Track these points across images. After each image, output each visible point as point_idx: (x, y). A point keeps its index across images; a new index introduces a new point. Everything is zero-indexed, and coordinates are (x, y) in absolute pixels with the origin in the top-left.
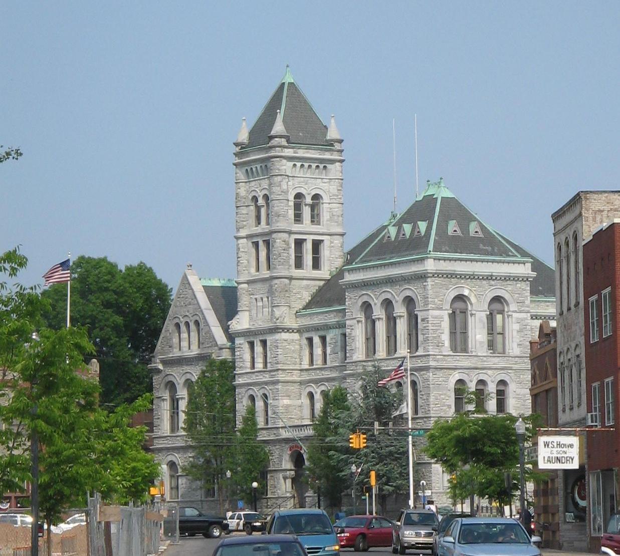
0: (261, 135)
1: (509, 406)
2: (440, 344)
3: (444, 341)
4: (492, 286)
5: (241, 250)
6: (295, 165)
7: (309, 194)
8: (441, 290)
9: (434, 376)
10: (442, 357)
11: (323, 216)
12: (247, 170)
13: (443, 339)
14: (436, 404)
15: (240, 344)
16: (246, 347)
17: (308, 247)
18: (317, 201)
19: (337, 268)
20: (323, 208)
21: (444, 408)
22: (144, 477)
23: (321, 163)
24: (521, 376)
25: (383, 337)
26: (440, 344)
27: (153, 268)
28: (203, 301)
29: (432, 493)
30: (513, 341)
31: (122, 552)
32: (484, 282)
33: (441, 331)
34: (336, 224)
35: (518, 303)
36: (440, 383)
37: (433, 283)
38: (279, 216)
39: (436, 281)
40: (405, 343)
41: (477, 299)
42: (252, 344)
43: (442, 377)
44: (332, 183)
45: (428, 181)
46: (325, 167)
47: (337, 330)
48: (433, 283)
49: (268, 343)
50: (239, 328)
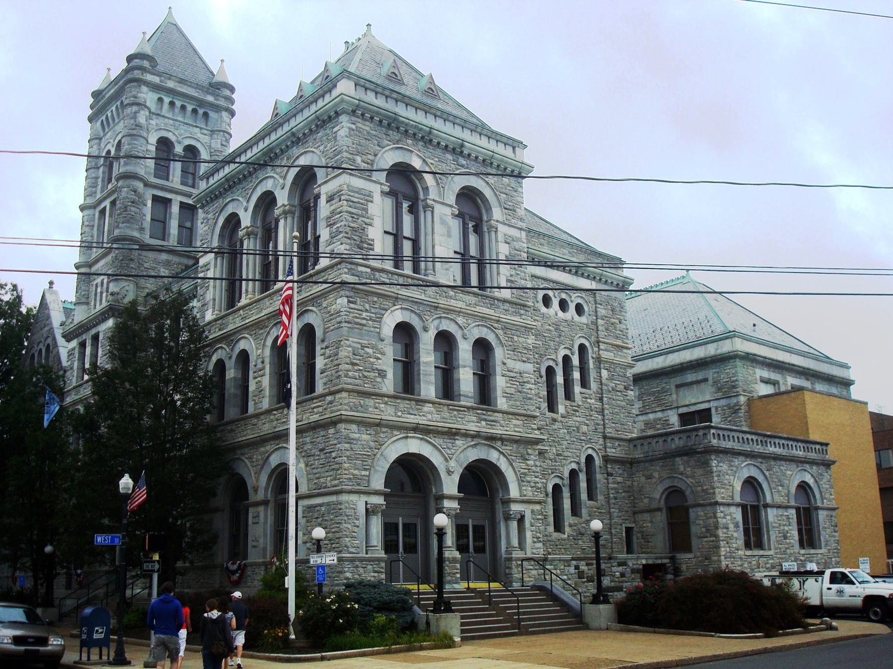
1: (495, 390)
2: (366, 246)
3: (373, 240)
4: (463, 166)
6: (160, 100)
7: (179, 143)
8: (368, 142)
9: (352, 306)
10: (368, 270)
13: (370, 237)
14: (356, 364)
18: (285, 427)
21: (372, 374)
23: (200, 106)
24: (516, 338)
26: (366, 246)
29: (340, 560)
30: (498, 274)
32: (449, 157)
33: (367, 221)
35: (505, 208)
36: (364, 322)
37: (354, 127)
39: (360, 125)
41: (437, 181)
43: (367, 311)
44: (215, 136)
46: (206, 115)
48: (354, 127)
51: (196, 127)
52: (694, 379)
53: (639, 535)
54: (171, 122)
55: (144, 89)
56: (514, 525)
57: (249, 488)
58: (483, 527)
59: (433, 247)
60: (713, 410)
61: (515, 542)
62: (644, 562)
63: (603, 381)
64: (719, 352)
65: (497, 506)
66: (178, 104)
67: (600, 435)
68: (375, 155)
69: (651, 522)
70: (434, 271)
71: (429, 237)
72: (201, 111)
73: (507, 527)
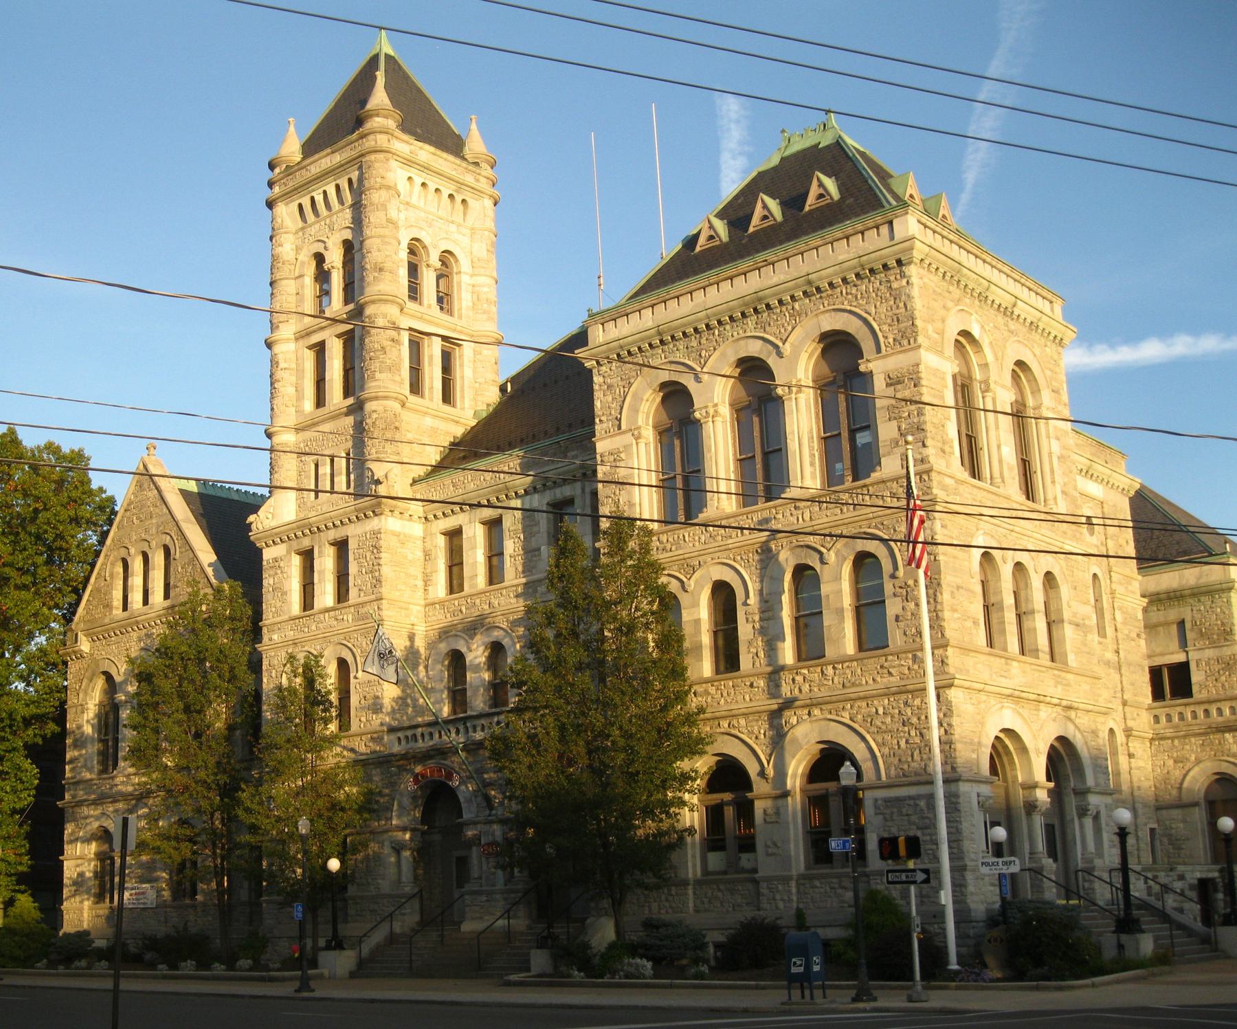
0: (345, 120)
5: (282, 365)
11: (460, 299)
12: (300, 206)
15: (276, 560)
16: (295, 564)
17: (433, 351)
19: (488, 405)
20: (459, 284)
22: (234, 633)
25: (727, 459)
27: (87, 453)
28: (181, 510)
31: (8, 980)
34: (485, 316)
38: (381, 270)
40: (812, 464)
42: (308, 556)
45: (783, 131)
47: (536, 496)
49: (352, 545)
50: (274, 524)
51: (452, 222)
52: (1162, 619)
53: (1165, 840)
54: (423, 214)
55: (394, 164)
56: (1088, 822)
57: (462, 800)
58: (1053, 826)
59: (999, 447)
60: (1193, 666)
61: (1091, 847)
62: (1198, 875)
63: (1119, 626)
64: (1203, 581)
65: (1066, 799)
66: (432, 186)
67: (1119, 701)
68: (943, 321)
69: (1184, 821)
70: (1003, 481)
71: (992, 433)
72: (458, 198)
73: (1082, 826)
